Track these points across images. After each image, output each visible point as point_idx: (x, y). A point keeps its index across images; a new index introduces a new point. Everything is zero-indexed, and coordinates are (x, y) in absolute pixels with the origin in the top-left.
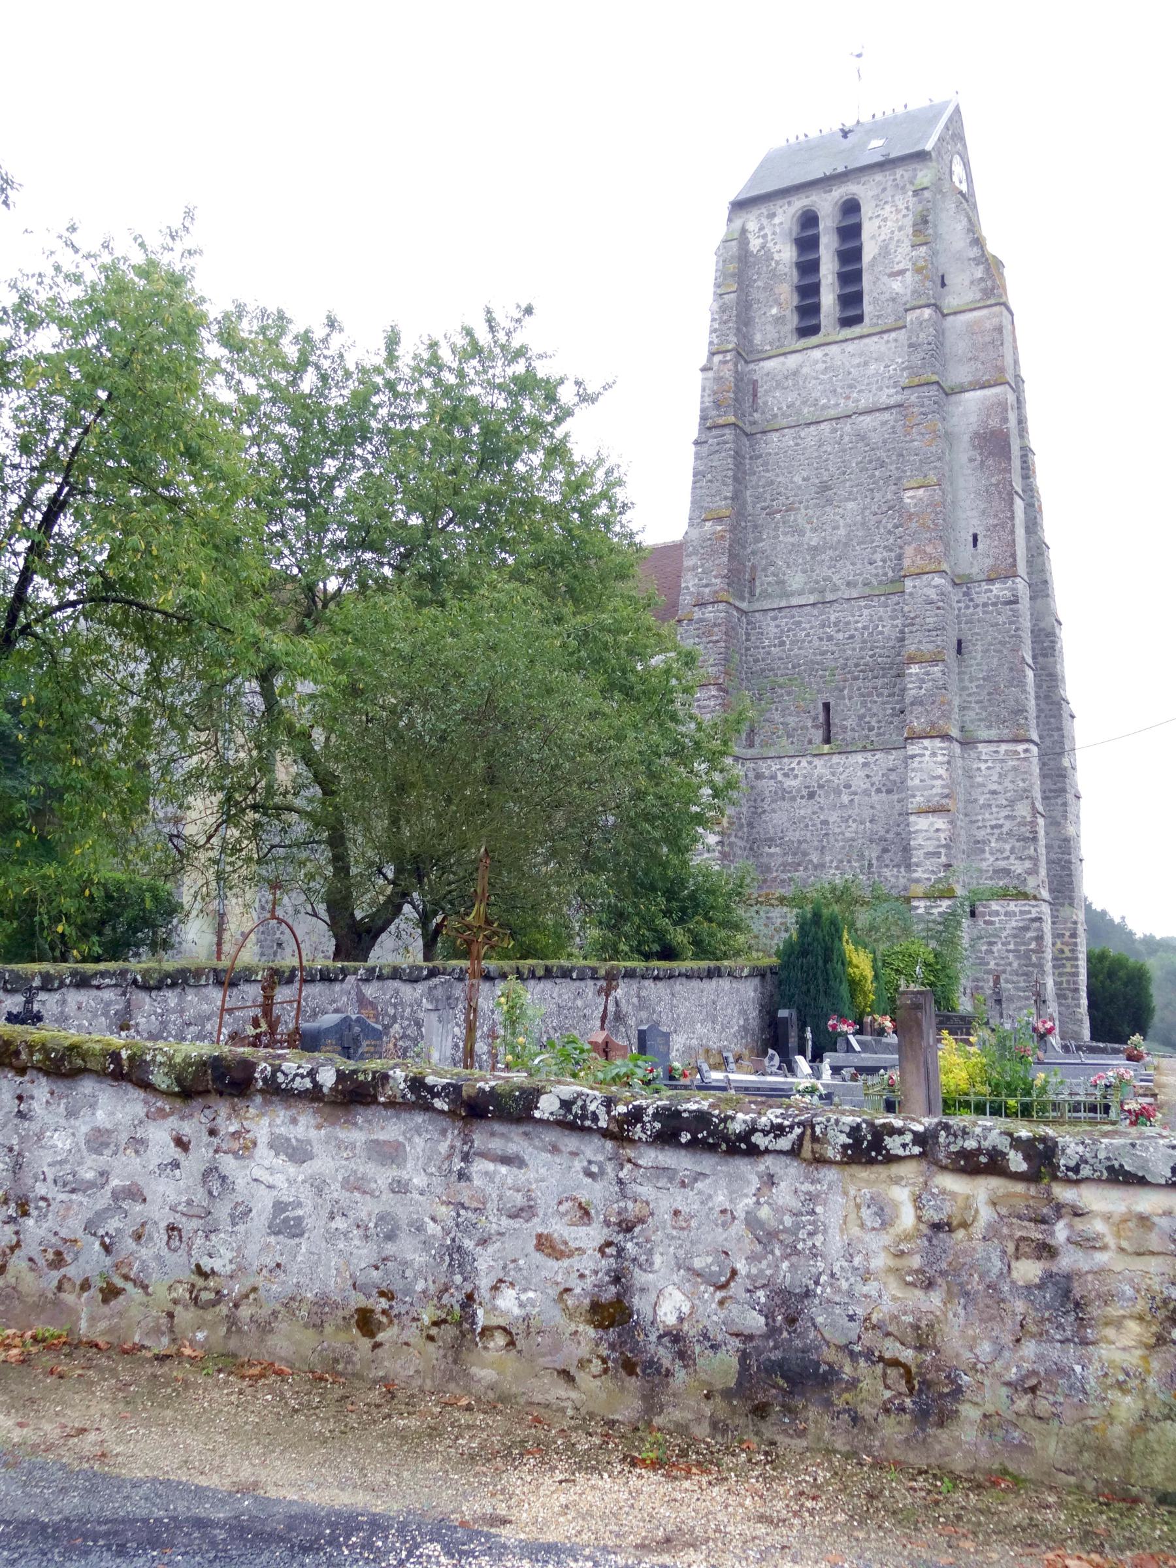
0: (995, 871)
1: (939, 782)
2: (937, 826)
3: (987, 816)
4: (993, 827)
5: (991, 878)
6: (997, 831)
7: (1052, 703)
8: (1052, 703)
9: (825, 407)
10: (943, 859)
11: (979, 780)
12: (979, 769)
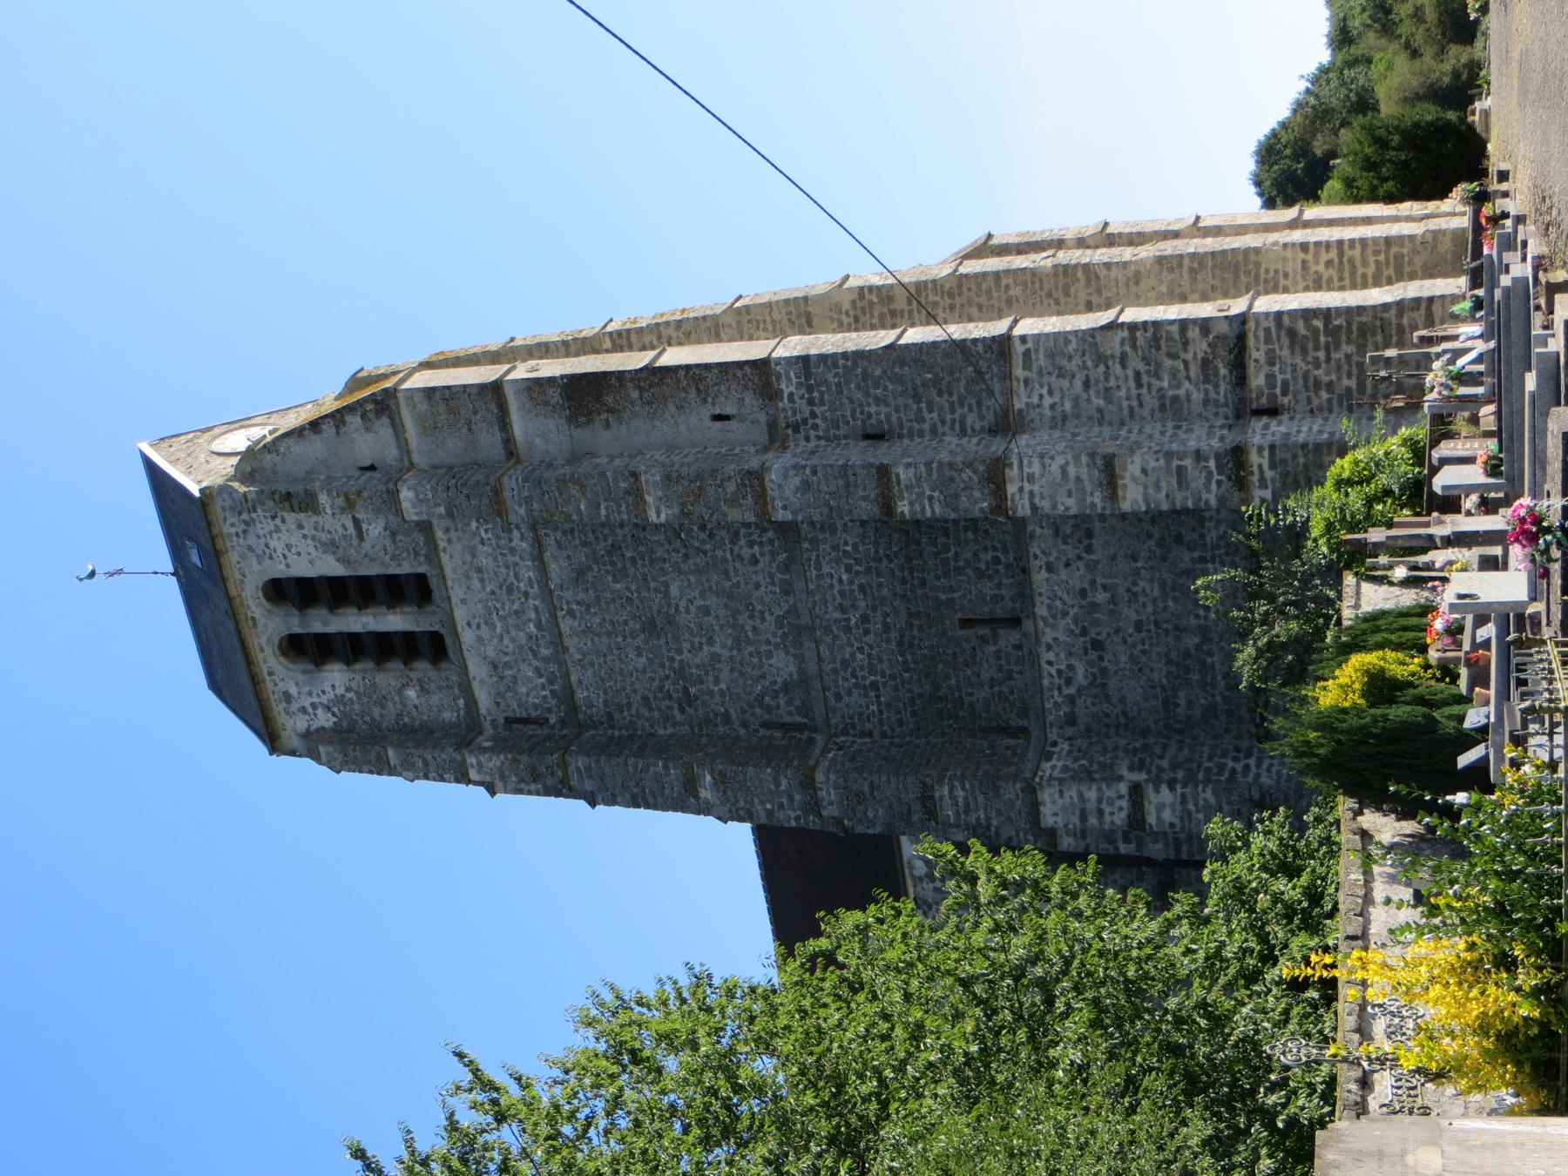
0: (1207, 380)
1: (1072, 470)
2: (1137, 472)
3: (1123, 393)
4: (1139, 385)
5: (1216, 386)
6: (1145, 379)
7: (960, 286)
8: (960, 286)
9: (539, 626)
10: (1188, 462)
11: (1068, 406)
12: (1052, 407)
